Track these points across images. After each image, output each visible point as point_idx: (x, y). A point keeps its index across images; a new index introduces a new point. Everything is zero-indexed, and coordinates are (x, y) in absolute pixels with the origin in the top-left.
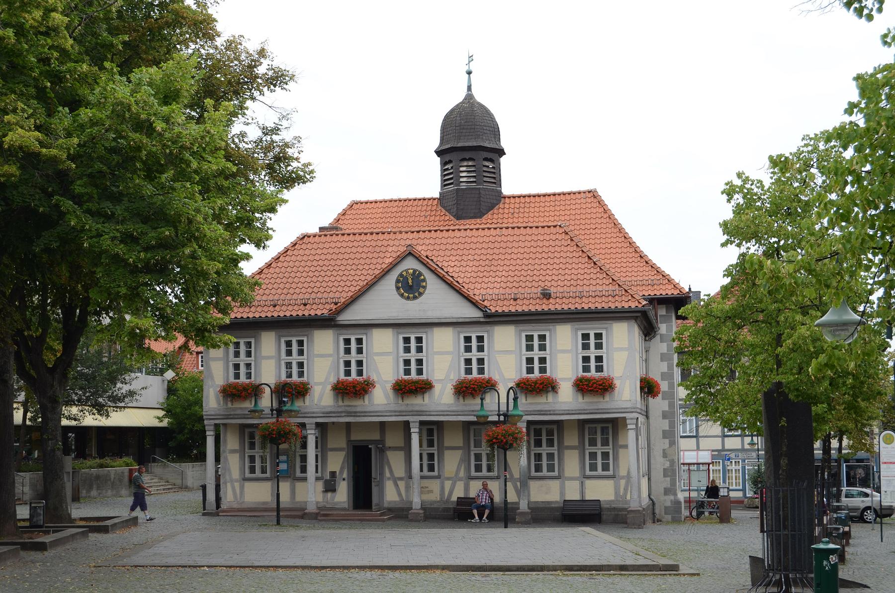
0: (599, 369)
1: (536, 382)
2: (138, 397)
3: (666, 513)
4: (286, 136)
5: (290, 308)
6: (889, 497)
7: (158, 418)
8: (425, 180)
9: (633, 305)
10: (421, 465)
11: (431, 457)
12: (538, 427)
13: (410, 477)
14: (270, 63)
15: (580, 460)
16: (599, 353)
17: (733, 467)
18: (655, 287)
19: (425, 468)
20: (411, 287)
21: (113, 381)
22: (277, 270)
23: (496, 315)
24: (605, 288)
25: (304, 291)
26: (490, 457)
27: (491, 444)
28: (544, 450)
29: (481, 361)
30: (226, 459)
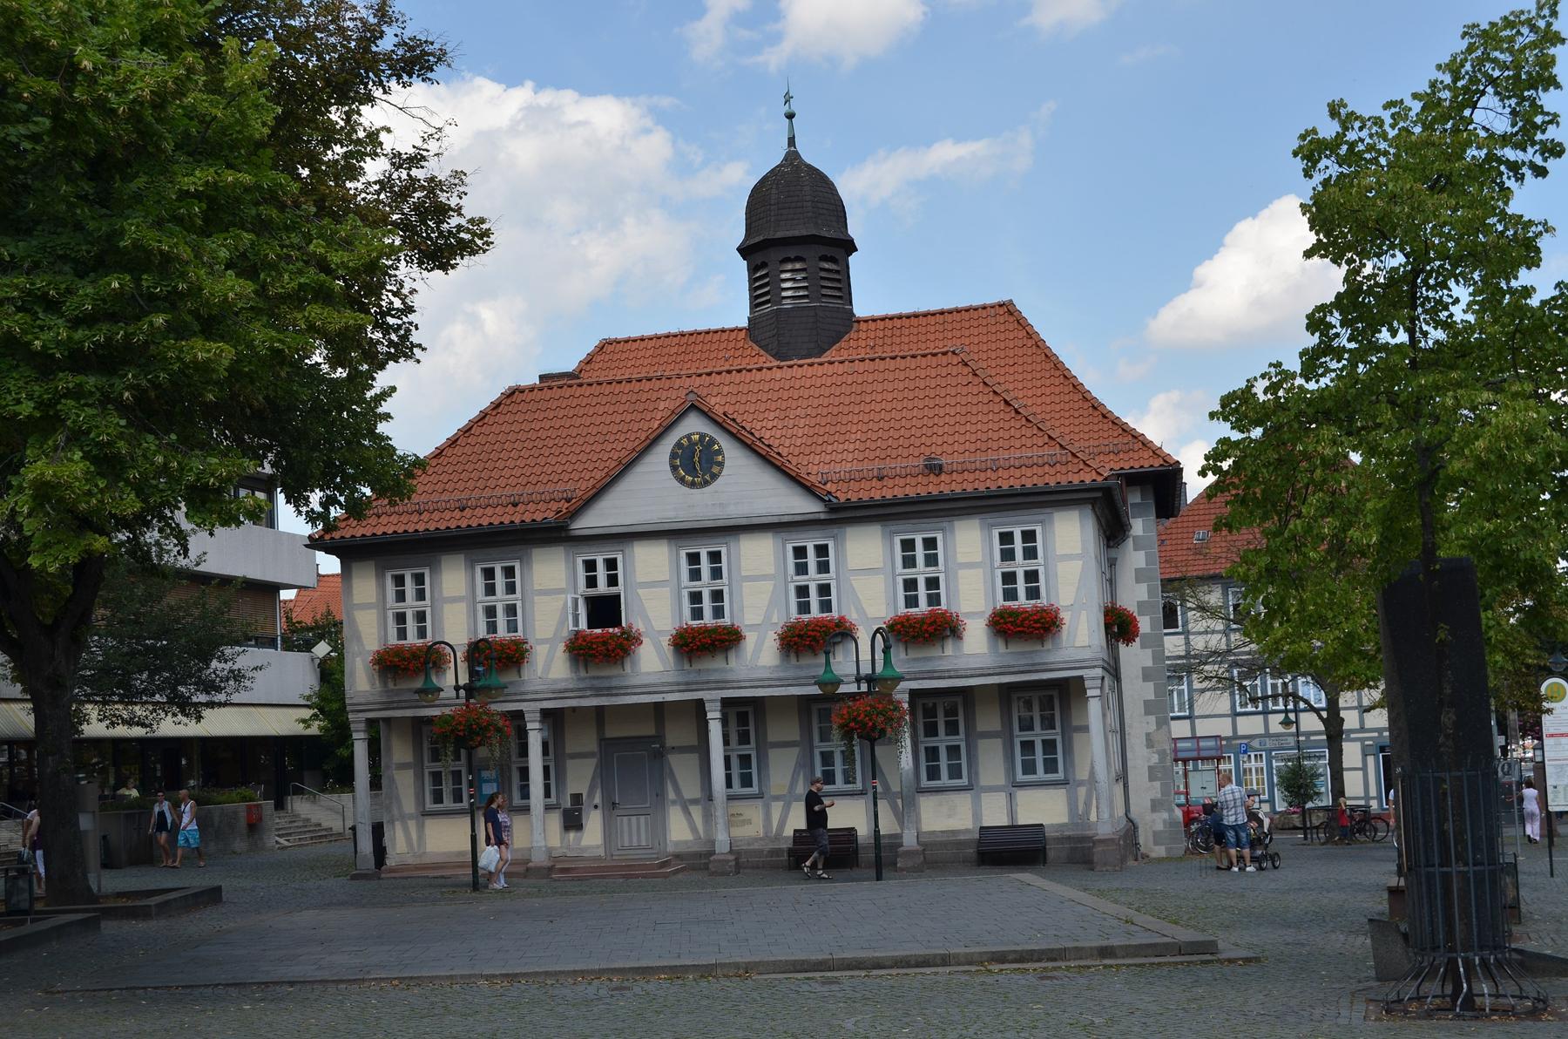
0: (1033, 593)
3: (1156, 843)
4: (435, 168)
5: (489, 511)
6: (1561, 795)
7: (304, 721)
9: (1088, 478)
11: (745, 760)
12: (930, 702)
13: (710, 798)
16: (1031, 565)
17: (1253, 764)
18: (1121, 455)
19: (736, 781)
20: (696, 465)
22: (468, 450)
23: (848, 506)
24: (1037, 452)
25: (513, 481)
26: (848, 758)
27: (847, 734)
28: (942, 741)
29: (824, 590)
30: (392, 780)
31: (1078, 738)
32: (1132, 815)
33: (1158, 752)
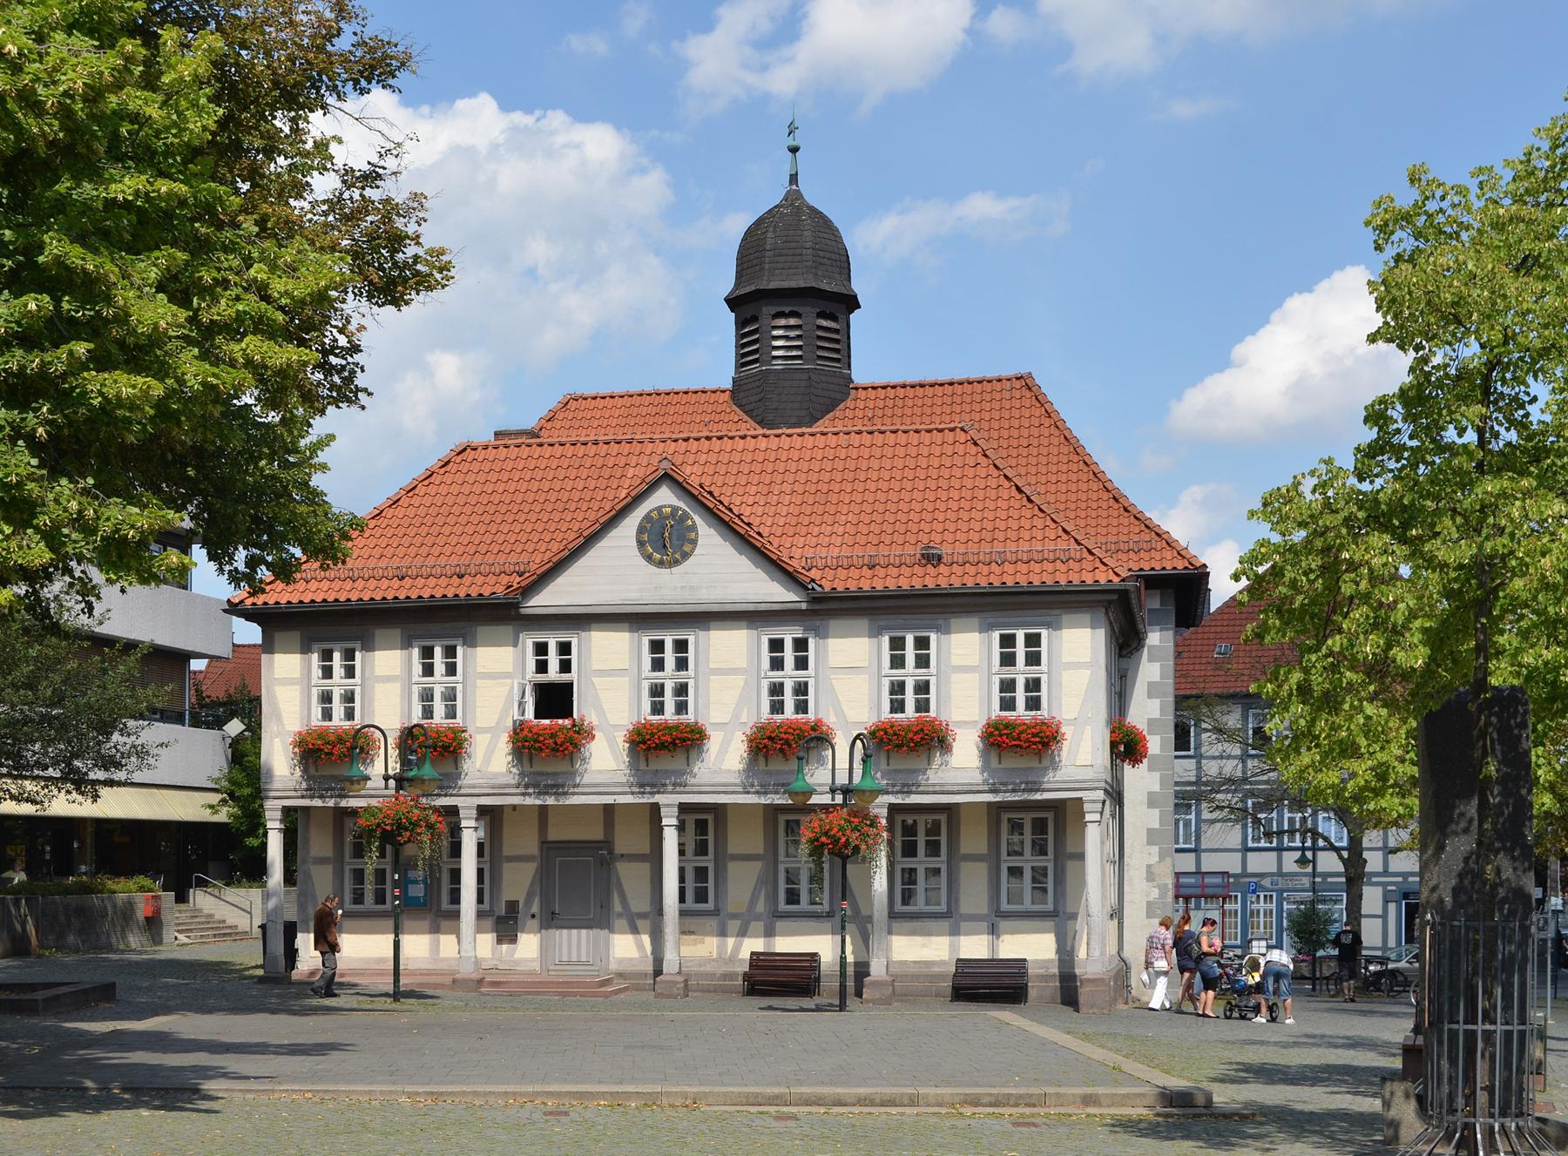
0: (1034, 704)
1: (907, 728)
2: (151, 761)
5: (432, 581)
7: (212, 807)
8: (711, 359)
9: (1103, 577)
10: (682, 891)
11: (701, 873)
14: (358, 29)
15: (990, 882)
18: (1142, 554)
20: (666, 543)
21: (106, 729)
26: (816, 878)
29: (801, 689)
30: (308, 876)
31: (1071, 865)
32: (1126, 954)
33: (1158, 886)
